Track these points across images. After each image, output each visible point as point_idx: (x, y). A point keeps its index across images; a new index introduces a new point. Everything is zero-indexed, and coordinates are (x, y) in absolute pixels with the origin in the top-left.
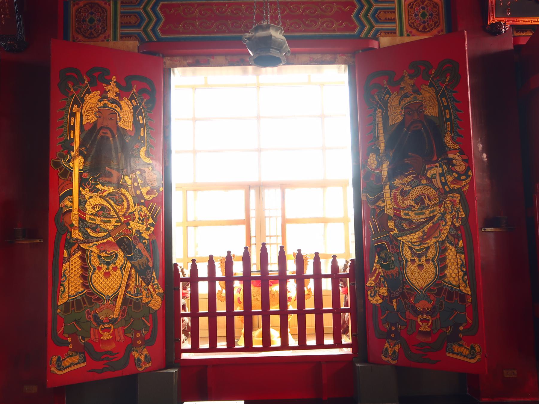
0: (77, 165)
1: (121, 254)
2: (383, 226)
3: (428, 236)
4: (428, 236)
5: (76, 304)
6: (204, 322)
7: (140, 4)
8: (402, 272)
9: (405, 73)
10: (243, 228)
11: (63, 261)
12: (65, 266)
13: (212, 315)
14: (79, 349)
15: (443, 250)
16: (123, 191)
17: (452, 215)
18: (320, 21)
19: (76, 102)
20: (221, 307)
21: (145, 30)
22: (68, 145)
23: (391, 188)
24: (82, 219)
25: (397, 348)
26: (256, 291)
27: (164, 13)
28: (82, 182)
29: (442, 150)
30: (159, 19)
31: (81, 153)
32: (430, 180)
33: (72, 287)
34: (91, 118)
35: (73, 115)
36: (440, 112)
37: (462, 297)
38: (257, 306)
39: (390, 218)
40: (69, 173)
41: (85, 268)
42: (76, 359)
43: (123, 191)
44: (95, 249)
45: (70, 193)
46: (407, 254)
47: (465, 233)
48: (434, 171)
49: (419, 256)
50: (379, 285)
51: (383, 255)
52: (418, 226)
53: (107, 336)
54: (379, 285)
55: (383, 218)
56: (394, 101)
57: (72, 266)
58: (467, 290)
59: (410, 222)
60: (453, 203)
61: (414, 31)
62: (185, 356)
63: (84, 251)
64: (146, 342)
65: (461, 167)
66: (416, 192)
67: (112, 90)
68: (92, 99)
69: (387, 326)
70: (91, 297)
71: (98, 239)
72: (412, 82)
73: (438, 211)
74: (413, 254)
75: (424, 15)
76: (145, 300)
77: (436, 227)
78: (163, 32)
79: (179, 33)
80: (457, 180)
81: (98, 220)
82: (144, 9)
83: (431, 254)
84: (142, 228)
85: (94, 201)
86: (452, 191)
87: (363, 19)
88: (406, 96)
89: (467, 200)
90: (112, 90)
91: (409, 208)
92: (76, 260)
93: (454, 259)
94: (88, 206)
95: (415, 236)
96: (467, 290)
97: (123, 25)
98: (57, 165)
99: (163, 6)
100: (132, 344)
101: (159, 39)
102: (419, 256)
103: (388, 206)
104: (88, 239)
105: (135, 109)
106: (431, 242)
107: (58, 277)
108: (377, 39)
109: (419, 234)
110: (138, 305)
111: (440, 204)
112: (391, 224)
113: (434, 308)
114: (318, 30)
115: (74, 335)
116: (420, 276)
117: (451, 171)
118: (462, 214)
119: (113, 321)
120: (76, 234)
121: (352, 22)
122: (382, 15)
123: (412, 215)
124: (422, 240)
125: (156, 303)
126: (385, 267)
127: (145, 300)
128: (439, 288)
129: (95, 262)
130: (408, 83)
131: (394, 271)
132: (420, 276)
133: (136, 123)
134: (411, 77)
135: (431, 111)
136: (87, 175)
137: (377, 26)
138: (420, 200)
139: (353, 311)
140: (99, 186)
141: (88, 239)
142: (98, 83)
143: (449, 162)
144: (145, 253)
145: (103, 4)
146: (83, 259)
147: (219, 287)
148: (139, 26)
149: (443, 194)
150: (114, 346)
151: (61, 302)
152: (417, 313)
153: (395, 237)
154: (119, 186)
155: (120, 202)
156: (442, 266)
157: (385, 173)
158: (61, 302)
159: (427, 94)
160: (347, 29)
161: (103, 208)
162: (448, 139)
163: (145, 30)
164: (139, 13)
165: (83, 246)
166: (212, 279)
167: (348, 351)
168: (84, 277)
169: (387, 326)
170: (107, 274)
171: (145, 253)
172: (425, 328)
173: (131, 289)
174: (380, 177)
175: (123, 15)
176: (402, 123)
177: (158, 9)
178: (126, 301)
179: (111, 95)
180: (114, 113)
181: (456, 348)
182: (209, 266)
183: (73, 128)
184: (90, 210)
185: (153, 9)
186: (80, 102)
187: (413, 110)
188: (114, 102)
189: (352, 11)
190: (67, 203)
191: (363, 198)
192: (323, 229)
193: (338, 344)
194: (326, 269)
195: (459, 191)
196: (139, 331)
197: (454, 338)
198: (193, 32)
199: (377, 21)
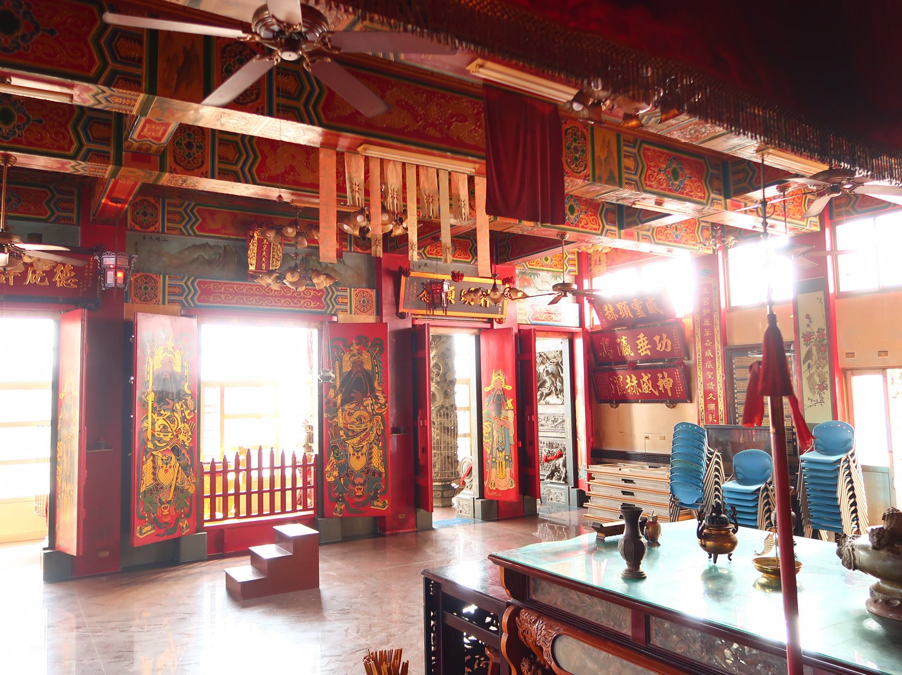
1: (174, 457)
2: (337, 435)
3: (363, 440)
4: (363, 440)
5: (150, 491)
7: (182, 279)
8: (347, 462)
9: (354, 342)
11: (143, 463)
12: (144, 467)
16: (176, 414)
17: (377, 427)
18: (303, 301)
21: (186, 299)
23: (343, 411)
24: (153, 435)
25: (342, 507)
27: (200, 287)
28: (154, 409)
29: (373, 390)
30: (196, 291)
32: (365, 407)
33: (147, 480)
36: (373, 368)
37: (380, 474)
39: (341, 429)
41: (154, 468)
42: (149, 528)
43: (176, 414)
44: (160, 455)
46: (351, 450)
47: (382, 438)
48: (368, 402)
49: (358, 452)
50: (333, 470)
51: (336, 451)
52: (358, 434)
53: (166, 512)
54: (333, 470)
55: (337, 428)
56: (346, 357)
57: (148, 467)
58: (383, 470)
59: (353, 431)
60: (377, 421)
62: (206, 525)
63: (154, 456)
64: (186, 516)
65: (382, 401)
66: (357, 414)
69: (337, 494)
70: (157, 487)
71: (162, 447)
72: (357, 347)
73: (369, 425)
74: (354, 450)
75: (364, 302)
77: (368, 434)
78: (199, 301)
79: (209, 302)
80: (380, 408)
81: (162, 434)
82: (186, 283)
83: (364, 450)
84: (185, 439)
86: (377, 414)
88: (354, 355)
89: (385, 420)
91: (353, 423)
92: (149, 463)
93: (376, 452)
94: (156, 426)
96: (383, 470)
97: (170, 294)
99: (199, 282)
100: (178, 518)
102: (358, 452)
103: (340, 421)
106: (364, 443)
109: (358, 438)
110: (182, 491)
111: (370, 421)
112: (342, 433)
113: (365, 481)
114: (301, 307)
115: (148, 512)
116: (357, 464)
117: (377, 403)
118: (382, 427)
121: (322, 303)
122: (340, 300)
124: (360, 442)
128: (368, 470)
129: (160, 463)
130: (355, 348)
131: (342, 461)
132: (357, 464)
133: (182, 366)
134: (357, 345)
135: (368, 367)
136: (156, 404)
137: (337, 307)
138: (359, 419)
139: (316, 487)
140: (162, 412)
141: (156, 448)
143: (376, 397)
144: (187, 456)
145: (154, 277)
146: (153, 461)
148: (182, 295)
151: (142, 490)
152: (355, 485)
153: (344, 441)
154: (173, 411)
155: (173, 422)
156: (370, 457)
157: (339, 402)
158: (142, 490)
159: (366, 356)
160: (319, 307)
161: (165, 427)
162: (376, 384)
163: (186, 299)
164: (181, 286)
165: (154, 453)
166: (237, 470)
167: (312, 512)
168: (154, 474)
169: (337, 494)
170: (166, 471)
171: (187, 456)
172: (359, 493)
173: (179, 480)
174: (335, 404)
175: (170, 286)
176: (351, 372)
177: (195, 284)
181: (376, 503)
184: (157, 429)
185: (192, 284)
187: (358, 364)
189: (322, 296)
190: (145, 424)
191: (325, 416)
193: (305, 508)
194: (289, 462)
195: (381, 414)
196: (183, 508)
197: (375, 498)
198: (220, 302)
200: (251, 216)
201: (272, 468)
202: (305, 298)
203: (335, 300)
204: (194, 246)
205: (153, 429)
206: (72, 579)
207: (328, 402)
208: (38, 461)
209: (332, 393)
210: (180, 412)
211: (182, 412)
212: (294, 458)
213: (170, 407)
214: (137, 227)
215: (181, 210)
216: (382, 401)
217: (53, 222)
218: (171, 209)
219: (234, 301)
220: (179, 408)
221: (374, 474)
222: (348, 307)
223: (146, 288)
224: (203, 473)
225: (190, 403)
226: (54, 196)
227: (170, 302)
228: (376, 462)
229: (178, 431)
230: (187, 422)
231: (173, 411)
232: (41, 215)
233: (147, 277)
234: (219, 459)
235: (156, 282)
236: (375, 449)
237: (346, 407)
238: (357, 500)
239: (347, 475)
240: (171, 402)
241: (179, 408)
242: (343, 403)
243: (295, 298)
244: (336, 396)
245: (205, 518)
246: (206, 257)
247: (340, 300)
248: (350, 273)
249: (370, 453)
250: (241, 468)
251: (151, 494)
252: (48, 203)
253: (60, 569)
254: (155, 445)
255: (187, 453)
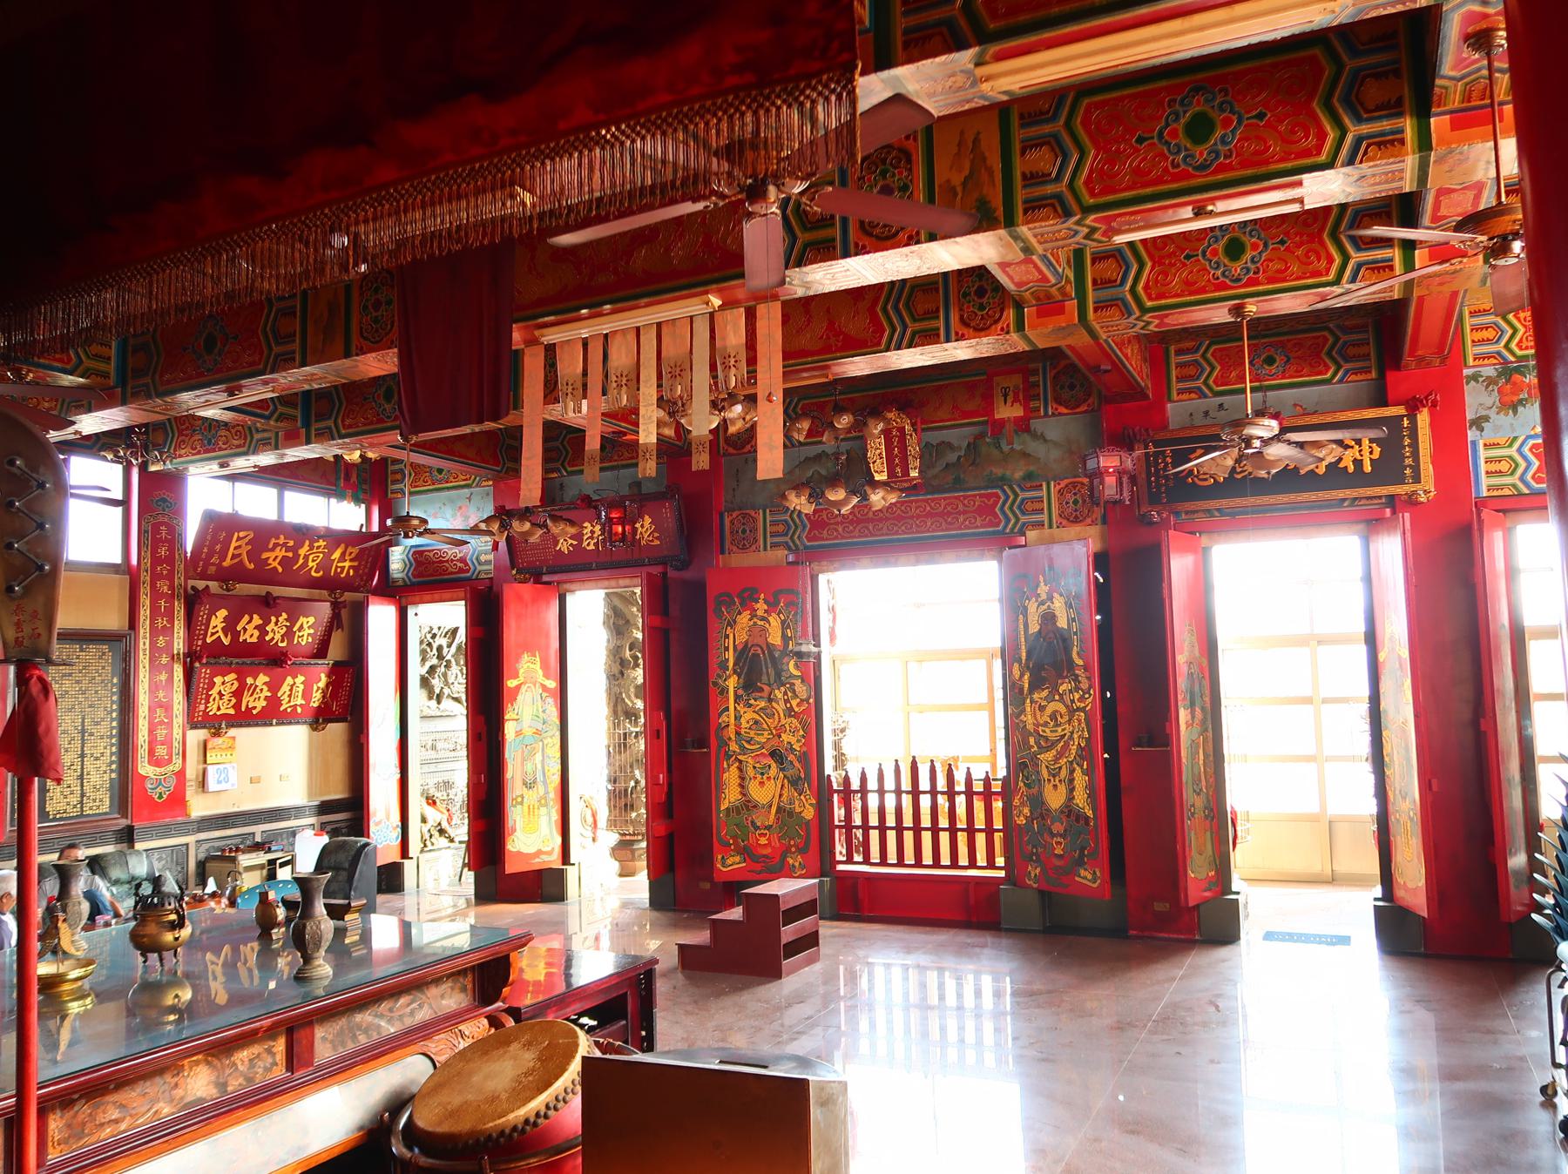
0: (732, 683)
3: (1060, 755)
4: (1060, 755)
5: (734, 810)
6: (874, 835)
8: (1041, 793)
10: (985, 714)
13: (882, 829)
14: (742, 851)
15: (1072, 771)
18: (961, 519)
19: (729, 624)
20: (944, 822)
22: (723, 665)
24: (738, 733)
26: (979, 805)
28: (737, 698)
31: (735, 672)
34: (742, 637)
35: (727, 637)
37: (1087, 819)
38: (980, 823)
40: (724, 691)
42: (737, 859)
45: (727, 709)
50: (1023, 804)
52: (1053, 744)
53: (763, 841)
54: (1023, 804)
55: (1025, 734)
57: (731, 776)
58: (1090, 813)
59: (1046, 739)
61: (1065, 522)
62: (840, 867)
65: (1085, 685)
67: (761, 607)
68: (744, 619)
70: (748, 805)
73: (1069, 728)
75: (1076, 502)
76: (798, 810)
80: (1082, 699)
81: (752, 733)
82: (1519, 451)
83: (1064, 773)
84: (793, 740)
85: (748, 716)
86: (1078, 709)
87: (1212, 360)
90: (761, 607)
91: (1046, 724)
92: (734, 770)
93: (1080, 780)
95: (1050, 755)
96: (1090, 813)
98: (715, 684)
100: (786, 850)
101: (806, 547)
104: (744, 750)
105: (783, 622)
107: (720, 787)
108: (1024, 534)
109: (1054, 752)
110: (791, 814)
111: (1069, 721)
112: (1032, 741)
115: (735, 838)
116: (1055, 799)
117: (1077, 689)
119: (769, 828)
120: (734, 747)
121: (996, 516)
123: (1048, 733)
124: (1056, 760)
125: (809, 813)
126: (1028, 786)
127: (798, 810)
128: (1069, 810)
129: (751, 772)
131: (1034, 791)
132: (1055, 799)
133: (784, 636)
136: (740, 692)
137: (1023, 519)
138: (1053, 716)
141: (744, 750)
142: (748, 603)
143: (1076, 679)
146: (740, 769)
147: (942, 801)
149: (1072, 712)
150: (769, 850)
154: (770, 700)
160: (991, 524)
161: (756, 722)
162: (1075, 655)
167: (1002, 874)
168: (742, 786)
170: (762, 783)
171: (797, 764)
172: (1058, 851)
173: (784, 798)
175: (774, 523)
178: (779, 809)
179: (760, 613)
180: (764, 630)
181: (1082, 872)
182: (1371, 709)
183: (727, 649)
184: (744, 725)
186: (732, 623)
188: (763, 619)
189: (996, 503)
192: (974, 743)
197: (1080, 863)
199: (1023, 513)
200: (875, 396)
201: (898, 792)
202: (964, 512)
203: (1019, 507)
204: (807, 459)
205: (738, 726)
206: (1426, 956)
207: (1013, 685)
208: (1353, 758)
209: (1016, 672)
210: (782, 703)
211: (786, 701)
212: (969, 781)
213: (766, 694)
214: (731, 450)
215: (1197, 356)
216: (1085, 685)
217: (1341, 381)
218: (1477, 321)
219: (856, 533)
220: (780, 696)
221: (1077, 821)
222: (1045, 517)
223: (744, 531)
224: (831, 791)
225: (800, 688)
226: (1337, 339)
227: (774, 545)
228: (1081, 798)
229: (781, 729)
230: (796, 716)
231: (770, 700)
232: (1320, 373)
233: (745, 515)
234: (978, 774)
235: (755, 520)
236: (1078, 773)
237: (1036, 696)
238: (1057, 862)
239: (1042, 817)
240: (767, 689)
241: (780, 696)
242: (1031, 691)
243: (949, 514)
244: (1022, 675)
245: (839, 858)
246: (824, 472)
247: (1029, 506)
248: (1055, 454)
249: (1072, 780)
250: (957, 789)
251: (739, 813)
252: (1329, 354)
253: (1399, 932)
254: (742, 748)
255: (804, 762)
